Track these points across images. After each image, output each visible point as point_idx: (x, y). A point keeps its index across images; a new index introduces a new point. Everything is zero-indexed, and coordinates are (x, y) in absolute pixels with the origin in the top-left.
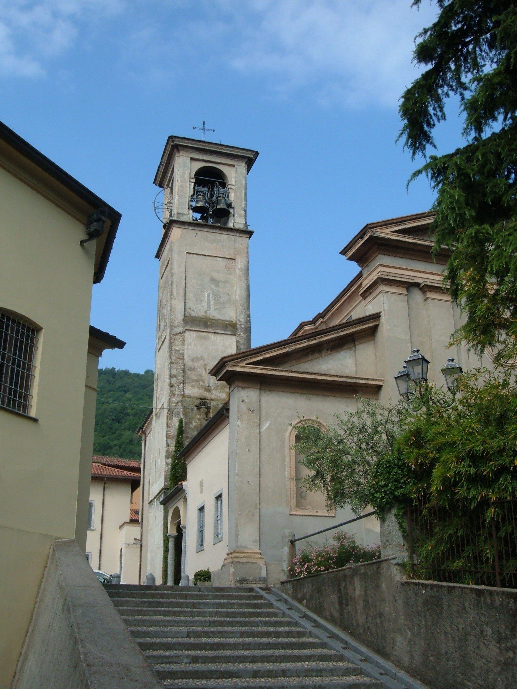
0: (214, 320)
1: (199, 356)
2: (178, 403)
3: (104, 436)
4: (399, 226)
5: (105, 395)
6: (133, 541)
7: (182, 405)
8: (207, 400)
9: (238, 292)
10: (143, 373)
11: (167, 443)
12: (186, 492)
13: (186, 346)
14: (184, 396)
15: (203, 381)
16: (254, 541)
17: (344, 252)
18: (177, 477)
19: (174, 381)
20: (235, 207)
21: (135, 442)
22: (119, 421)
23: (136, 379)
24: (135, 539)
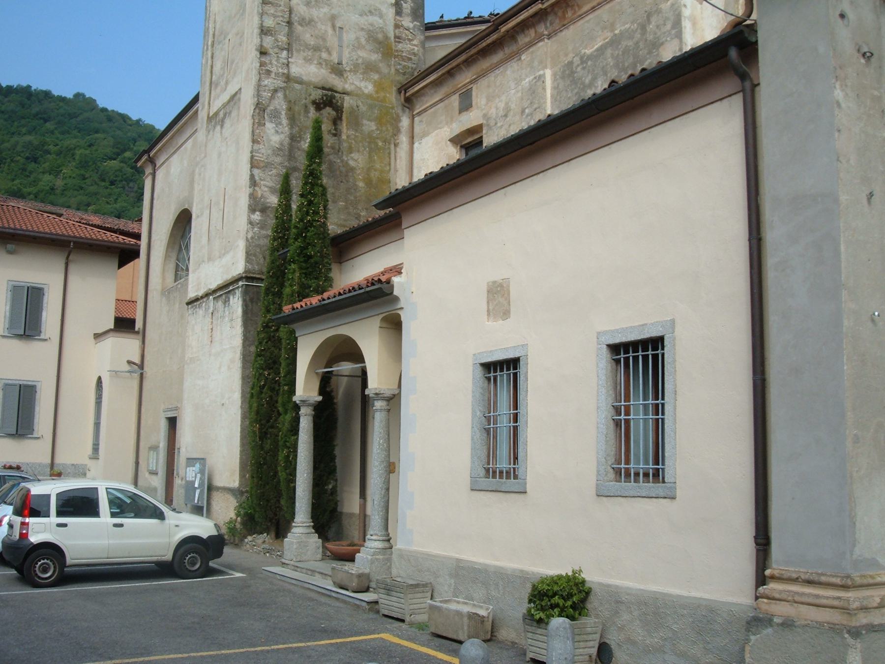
2: (275, 91)
3: (13, 180)
5: (16, 123)
6: (127, 367)
7: (285, 96)
8: (336, 92)
10: (71, 97)
11: (252, 177)
12: (402, 304)
14: (288, 78)
18: (310, 257)
19: (268, 41)
21: (58, 191)
22: (35, 160)
23: (61, 104)
24: (129, 362)
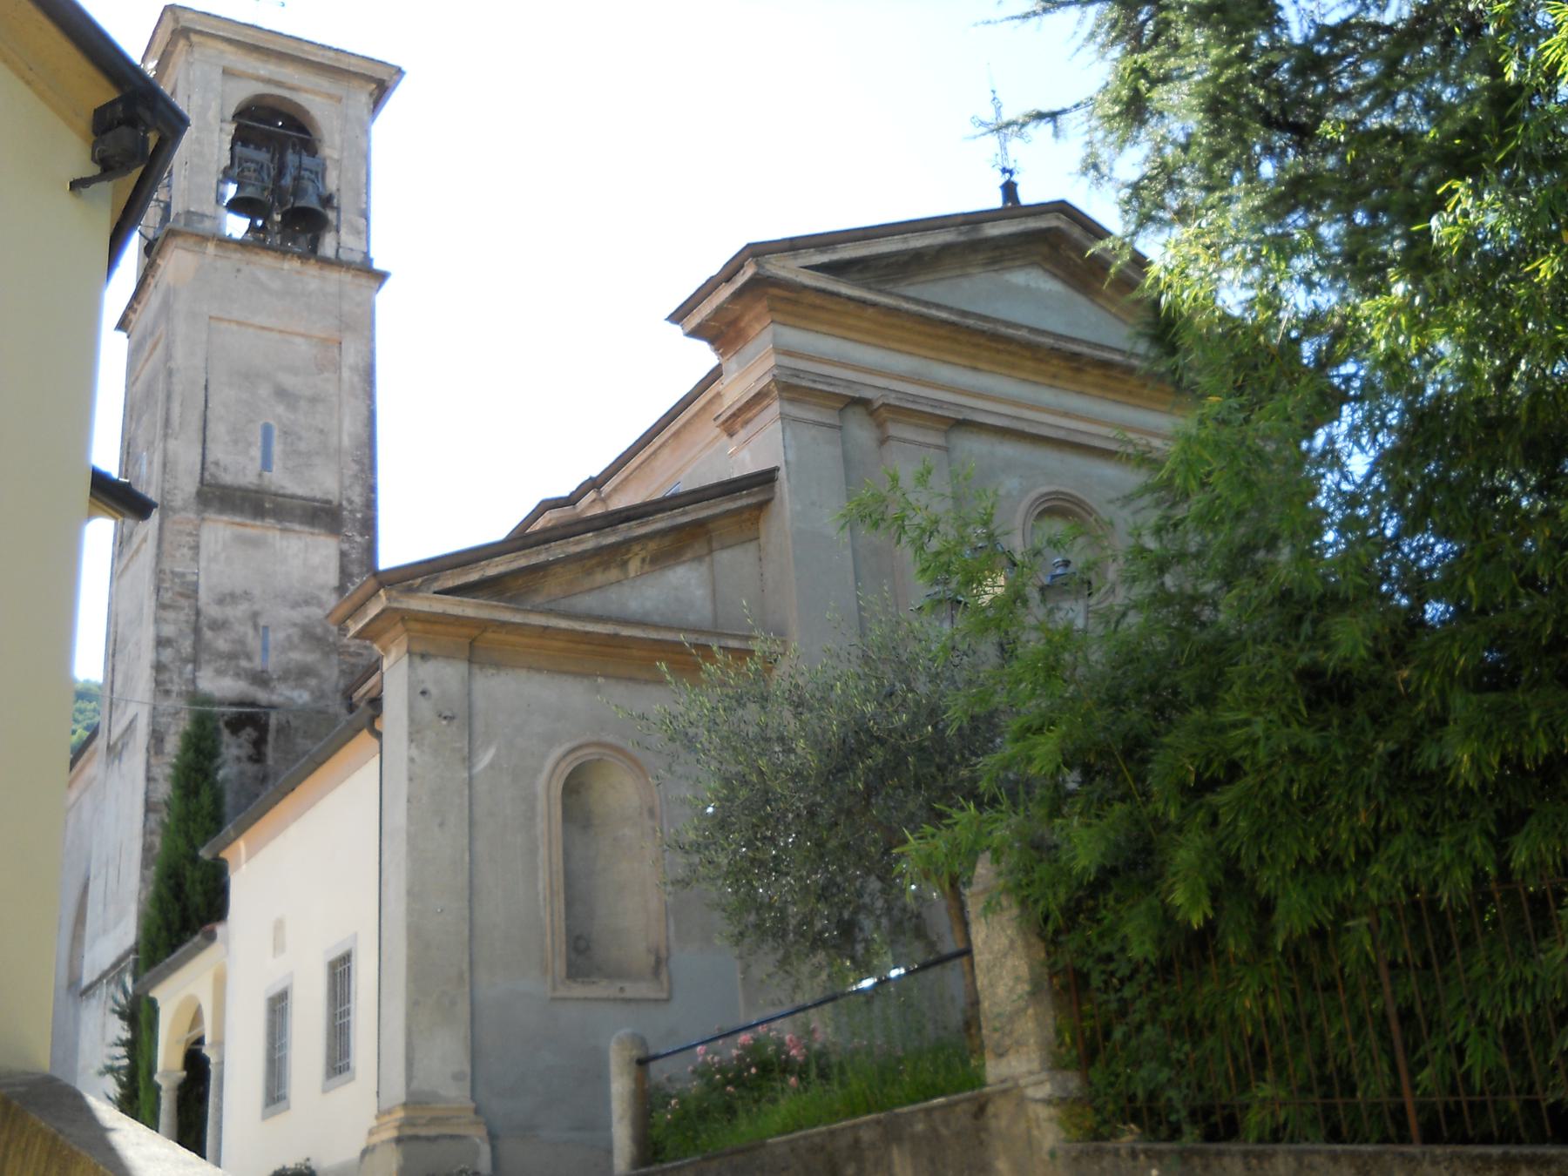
0: (284, 496)
1: (238, 591)
4: (822, 252)
9: (347, 425)
13: (203, 564)
15: (249, 657)
16: (457, 1077)
17: (677, 317)
19: (167, 654)
20: (343, 208)
